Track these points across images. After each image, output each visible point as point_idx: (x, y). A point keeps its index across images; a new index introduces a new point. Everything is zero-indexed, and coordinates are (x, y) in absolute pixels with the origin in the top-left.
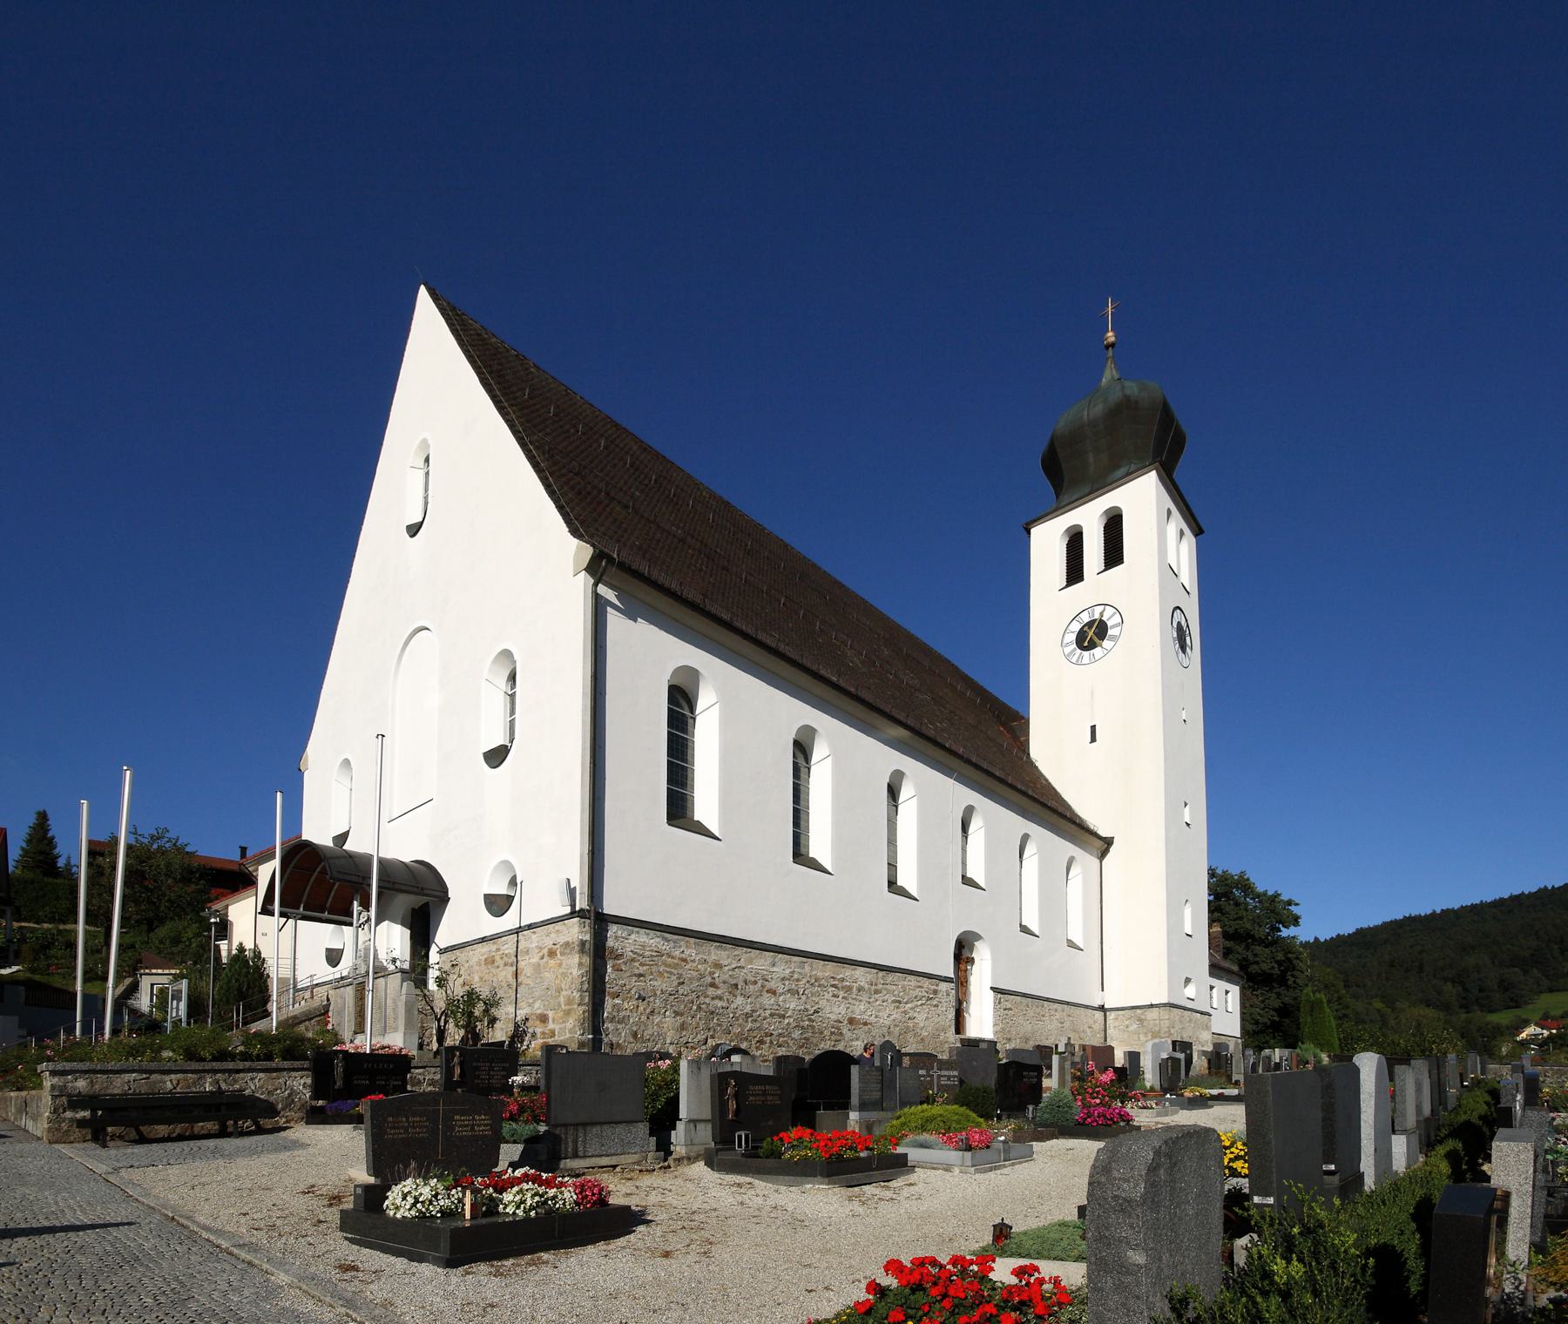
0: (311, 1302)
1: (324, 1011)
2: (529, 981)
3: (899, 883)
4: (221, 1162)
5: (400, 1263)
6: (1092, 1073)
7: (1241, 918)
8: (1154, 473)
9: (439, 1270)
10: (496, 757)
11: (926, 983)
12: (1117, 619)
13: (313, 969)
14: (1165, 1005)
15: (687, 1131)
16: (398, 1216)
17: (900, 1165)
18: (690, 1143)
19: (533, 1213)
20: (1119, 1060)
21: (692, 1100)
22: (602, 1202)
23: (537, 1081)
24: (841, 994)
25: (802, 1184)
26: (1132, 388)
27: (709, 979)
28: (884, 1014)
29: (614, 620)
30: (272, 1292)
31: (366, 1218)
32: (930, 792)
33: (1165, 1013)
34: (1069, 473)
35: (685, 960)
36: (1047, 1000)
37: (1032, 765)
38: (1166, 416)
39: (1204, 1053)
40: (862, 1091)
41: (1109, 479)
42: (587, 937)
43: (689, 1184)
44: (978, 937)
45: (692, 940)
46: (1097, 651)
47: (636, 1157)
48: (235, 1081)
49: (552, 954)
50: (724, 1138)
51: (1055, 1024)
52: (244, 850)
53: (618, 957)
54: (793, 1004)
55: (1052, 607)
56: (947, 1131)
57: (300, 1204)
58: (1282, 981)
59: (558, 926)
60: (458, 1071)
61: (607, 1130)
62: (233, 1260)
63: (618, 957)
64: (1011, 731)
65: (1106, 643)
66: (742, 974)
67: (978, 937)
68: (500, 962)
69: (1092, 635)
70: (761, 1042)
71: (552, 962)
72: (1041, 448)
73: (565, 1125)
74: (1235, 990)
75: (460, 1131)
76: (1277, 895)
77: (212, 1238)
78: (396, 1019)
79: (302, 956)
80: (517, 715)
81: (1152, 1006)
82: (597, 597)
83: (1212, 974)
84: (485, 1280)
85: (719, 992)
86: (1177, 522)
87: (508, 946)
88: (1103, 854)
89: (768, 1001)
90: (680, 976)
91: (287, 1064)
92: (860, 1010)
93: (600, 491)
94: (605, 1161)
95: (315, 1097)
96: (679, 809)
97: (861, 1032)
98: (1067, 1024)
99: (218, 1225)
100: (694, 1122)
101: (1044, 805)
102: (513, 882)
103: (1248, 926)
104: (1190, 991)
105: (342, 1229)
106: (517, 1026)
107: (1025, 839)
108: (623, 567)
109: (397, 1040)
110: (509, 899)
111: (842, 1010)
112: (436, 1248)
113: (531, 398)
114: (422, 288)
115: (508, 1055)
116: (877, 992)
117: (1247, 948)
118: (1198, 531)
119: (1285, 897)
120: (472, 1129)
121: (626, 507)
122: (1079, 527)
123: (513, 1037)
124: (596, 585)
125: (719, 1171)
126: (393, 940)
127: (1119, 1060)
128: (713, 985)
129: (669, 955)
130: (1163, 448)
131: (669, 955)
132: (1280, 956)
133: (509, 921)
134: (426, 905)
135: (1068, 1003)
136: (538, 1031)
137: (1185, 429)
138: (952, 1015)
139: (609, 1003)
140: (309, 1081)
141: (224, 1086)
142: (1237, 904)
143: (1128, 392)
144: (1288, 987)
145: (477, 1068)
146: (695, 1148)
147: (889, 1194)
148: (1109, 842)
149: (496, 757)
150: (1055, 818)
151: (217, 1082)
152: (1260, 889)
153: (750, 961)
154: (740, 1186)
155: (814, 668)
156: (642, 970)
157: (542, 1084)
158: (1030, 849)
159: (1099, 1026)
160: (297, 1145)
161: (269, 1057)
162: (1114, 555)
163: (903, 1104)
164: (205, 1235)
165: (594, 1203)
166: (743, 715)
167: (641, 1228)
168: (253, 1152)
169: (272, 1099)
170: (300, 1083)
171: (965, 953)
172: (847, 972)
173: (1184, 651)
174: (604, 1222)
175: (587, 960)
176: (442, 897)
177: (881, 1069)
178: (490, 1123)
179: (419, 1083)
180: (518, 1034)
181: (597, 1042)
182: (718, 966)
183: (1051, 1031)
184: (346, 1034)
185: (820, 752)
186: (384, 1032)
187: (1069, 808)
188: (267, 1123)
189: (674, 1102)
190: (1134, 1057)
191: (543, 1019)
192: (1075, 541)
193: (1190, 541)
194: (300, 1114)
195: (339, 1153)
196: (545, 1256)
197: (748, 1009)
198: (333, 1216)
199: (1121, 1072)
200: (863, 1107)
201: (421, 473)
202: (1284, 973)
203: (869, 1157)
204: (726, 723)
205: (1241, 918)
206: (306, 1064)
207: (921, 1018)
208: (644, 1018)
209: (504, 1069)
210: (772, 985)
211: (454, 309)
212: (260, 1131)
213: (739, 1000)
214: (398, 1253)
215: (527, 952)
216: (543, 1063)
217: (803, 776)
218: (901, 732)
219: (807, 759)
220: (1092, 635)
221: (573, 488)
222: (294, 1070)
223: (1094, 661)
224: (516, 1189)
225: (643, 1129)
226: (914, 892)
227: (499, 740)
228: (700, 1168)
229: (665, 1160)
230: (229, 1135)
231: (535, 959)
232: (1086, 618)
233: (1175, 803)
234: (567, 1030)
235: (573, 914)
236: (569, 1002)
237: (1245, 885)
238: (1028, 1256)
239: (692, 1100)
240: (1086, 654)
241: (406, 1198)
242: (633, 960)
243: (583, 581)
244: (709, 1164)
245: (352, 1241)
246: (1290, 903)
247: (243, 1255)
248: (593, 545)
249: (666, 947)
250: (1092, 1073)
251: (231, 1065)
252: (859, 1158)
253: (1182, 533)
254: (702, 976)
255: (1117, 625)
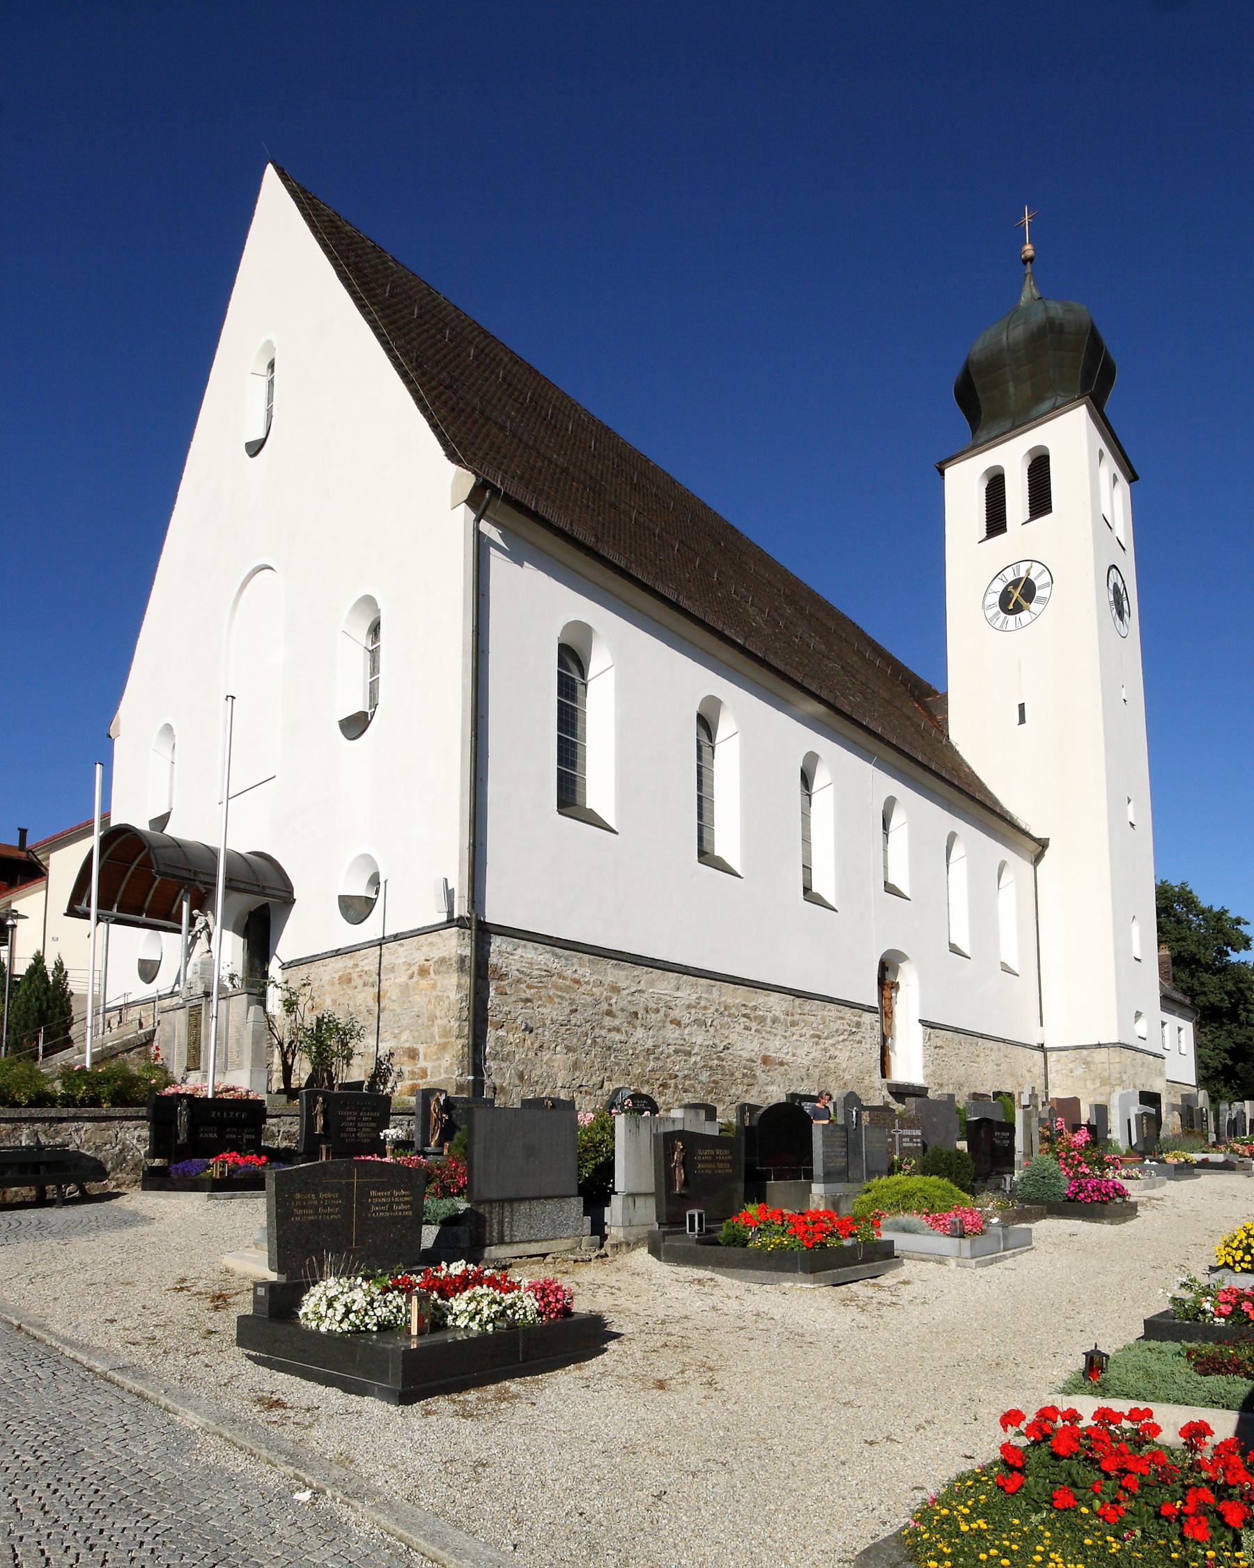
0: (241, 1457)
1: (150, 1038)
2: (395, 1006)
3: (814, 890)
4: (52, 1243)
5: (334, 1397)
6: (1060, 1133)
7: (1184, 939)
8: (1083, 409)
9: (392, 1408)
10: (355, 725)
11: (848, 1013)
12: (1045, 578)
13: (126, 985)
14: (1114, 1045)
15: (625, 1207)
16: (323, 1329)
17: (884, 1255)
18: (628, 1224)
19: (490, 1327)
20: (1086, 1115)
21: (631, 1166)
22: (566, 1312)
23: (409, 1134)
24: (754, 1026)
25: (779, 1281)
26: (1056, 309)
27: (605, 1006)
28: (801, 1052)
29: (499, 564)
30: (181, 1441)
31: (273, 1327)
32: (850, 779)
33: (1115, 1055)
34: (985, 407)
35: (577, 982)
36: (982, 1036)
37: (951, 748)
38: (1095, 345)
39: (1174, 1107)
40: (826, 1156)
41: (1034, 413)
42: (467, 952)
43: (637, 1279)
44: (904, 957)
45: (586, 957)
46: (1024, 615)
47: (569, 1243)
48: (57, 1133)
49: (423, 972)
50: (671, 1219)
51: (991, 1067)
52: (23, 832)
53: (502, 977)
54: (699, 1038)
55: (972, 564)
56: (932, 1210)
57: (177, 1306)
58: (1233, 1015)
59: (432, 937)
60: (320, 1121)
61: (537, 1207)
62: (116, 1391)
63: (502, 977)
64: (926, 707)
65: (1034, 606)
66: (641, 1000)
67: (904, 957)
68: (357, 981)
69: (1017, 597)
70: (664, 1085)
71: (423, 983)
72: (955, 373)
73: (490, 1202)
74: (1188, 1027)
75: (378, 1212)
76: (1224, 912)
77: (80, 1357)
78: (240, 1053)
79: (111, 968)
80: (382, 675)
81: (1099, 1046)
82: (479, 535)
83: (1164, 1008)
84: (454, 1422)
85: (617, 1022)
86: (1109, 467)
87: (368, 960)
88: (1037, 859)
89: (672, 1033)
90: (572, 1002)
91: (118, 1111)
92: (776, 1046)
93: (474, 409)
94: (534, 1248)
95: (153, 1154)
96: (569, 796)
97: (777, 1073)
98: (1004, 1067)
99: (80, 1337)
100: (632, 1196)
101: (973, 798)
102: (375, 881)
103: (1193, 948)
104: (1141, 1028)
105: (240, 1342)
106: (379, 1063)
107: (952, 837)
108: (509, 500)
109: (241, 1080)
110: (369, 903)
111: (755, 1045)
112: (382, 1375)
113: (392, 296)
114: (270, 168)
115: (371, 1102)
116: (793, 1024)
117: (1192, 975)
118: (1132, 477)
119: (1232, 915)
120: (391, 1209)
121: (503, 428)
122: (1000, 468)
123: (374, 1077)
124: (478, 520)
125: (666, 1261)
126: (229, 951)
127: (1086, 1115)
128: (609, 1013)
129: (560, 976)
130: (1090, 376)
131: (560, 976)
132: (1230, 986)
133: (370, 929)
134: (265, 907)
135: (1004, 1041)
136: (406, 1069)
137: (1115, 358)
138: (877, 1054)
139: (491, 1034)
140: (146, 1133)
141: (43, 1140)
142: (1179, 922)
143: (1052, 313)
144: (1240, 1025)
145: (344, 1118)
146: (635, 1230)
147: (885, 1296)
148: (1043, 844)
149: (355, 725)
150: (984, 814)
151: (36, 1134)
152: (1204, 903)
153: (652, 983)
154: (699, 1281)
155: (719, 626)
156: (529, 993)
157: (417, 1139)
158: (958, 850)
159: (1039, 1069)
160: (134, 1219)
161: (95, 1102)
162: (1040, 503)
163: (871, 1174)
164: (69, 1352)
165: (558, 1312)
166: (642, 679)
167: (612, 1345)
168: (87, 1229)
169: (100, 1156)
170: (135, 1137)
171: (889, 977)
172: (761, 998)
173: (1121, 618)
174: (568, 1338)
175: (467, 981)
176: (287, 900)
177: (845, 1128)
178: (415, 1206)
179: (273, 1136)
180: (380, 1074)
181: (478, 1085)
182: (616, 989)
183: (985, 1075)
184: (177, 1071)
185: (725, 728)
186: (224, 1068)
187: (996, 801)
188: (93, 1188)
189: (607, 1169)
190: (1101, 1111)
191: (413, 1054)
192: (996, 485)
193: (1123, 487)
194: (132, 1176)
195: (230, 1237)
196: (513, 1386)
197: (650, 1044)
198: (227, 1324)
199: (1091, 1129)
200: (828, 1177)
201: (264, 382)
202: (1235, 1007)
203: (854, 1247)
204: (624, 690)
205: (1184, 939)
206: (143, 1111)
207: (842, 1056)
208: (531, 1054)
209: (374, 1119)
210: (676, 1014)
211: (304, 191)
212: (86, 1198)
213: (640, 1033)
214: (328, 1381)
215: (392, 969)
216: (419, 1112)
217: (705, 755)
218: (820, 709)
219: (711, 737)
220: (1017, 597)
221: (445, 404)
222: (127, 1118)
223: (1020, 626)
224: (467, 1294)
225: (577, 1204)
226: (831, 901)
227: (359, 704)
228: (642, 1257)
229: (601, 1246)
230: (50, 1203)
231: (403, 979)
232: (1010, 576)
233: (1118, 799)
234: (442, 1069)
235: (451, 922)
236: (446, 1033)
237: (1188, 900)
238: (1138, 1397)
239: (631, 1166)
240: (1011, 618)
241: (333, 1302)
242: (519, 981)
243: (463, 516)
244: (654, 1251)
245: (258, 1361)
246: (1238, 921)
247: (129, 1383)
248: (474, 472)
249: (555, 965)
250: (1060, 1133)
251: (53, 1113)
252: (842, 1246)
253: (1115, 479)
254: (597, 1002)
255: (1046, 585)
